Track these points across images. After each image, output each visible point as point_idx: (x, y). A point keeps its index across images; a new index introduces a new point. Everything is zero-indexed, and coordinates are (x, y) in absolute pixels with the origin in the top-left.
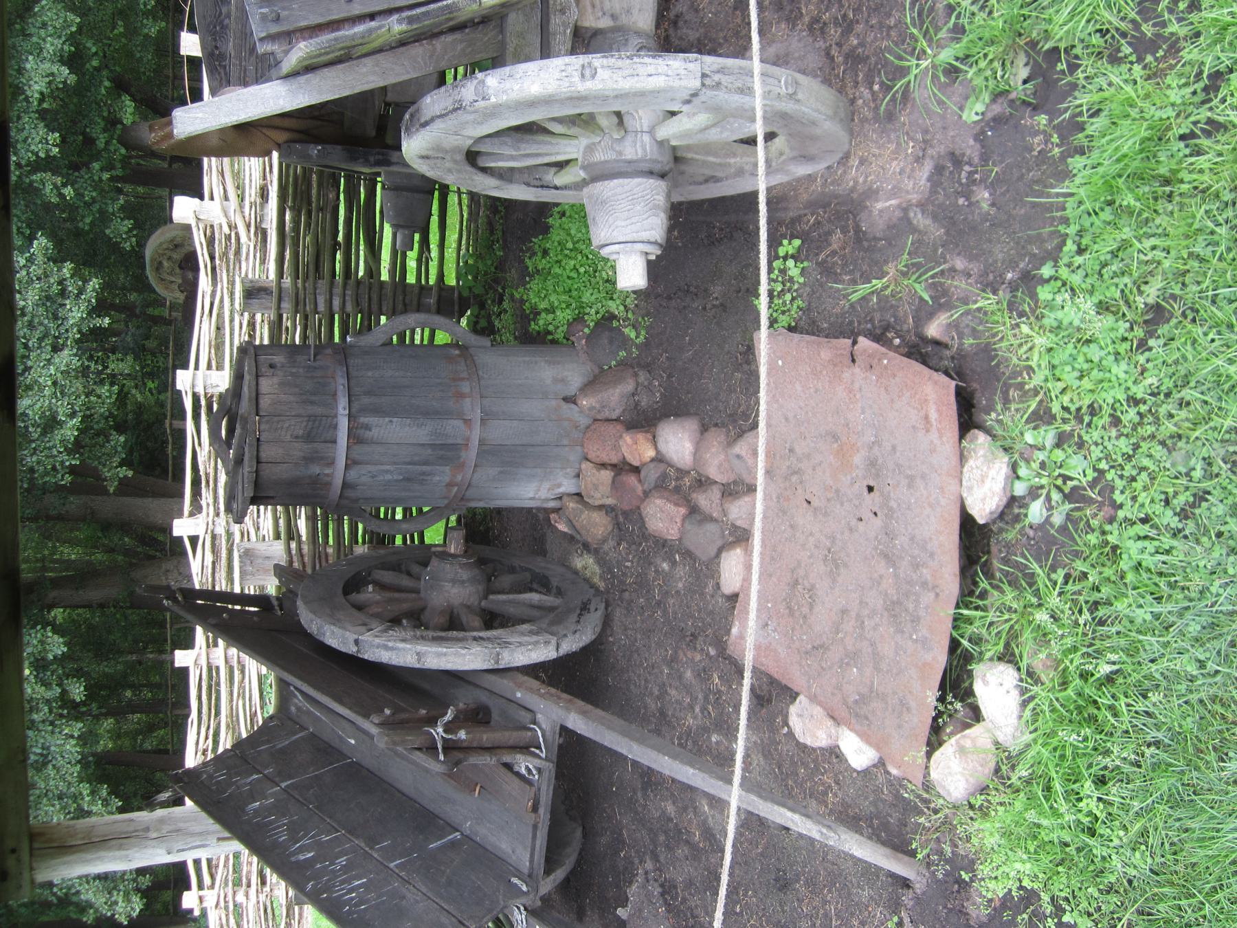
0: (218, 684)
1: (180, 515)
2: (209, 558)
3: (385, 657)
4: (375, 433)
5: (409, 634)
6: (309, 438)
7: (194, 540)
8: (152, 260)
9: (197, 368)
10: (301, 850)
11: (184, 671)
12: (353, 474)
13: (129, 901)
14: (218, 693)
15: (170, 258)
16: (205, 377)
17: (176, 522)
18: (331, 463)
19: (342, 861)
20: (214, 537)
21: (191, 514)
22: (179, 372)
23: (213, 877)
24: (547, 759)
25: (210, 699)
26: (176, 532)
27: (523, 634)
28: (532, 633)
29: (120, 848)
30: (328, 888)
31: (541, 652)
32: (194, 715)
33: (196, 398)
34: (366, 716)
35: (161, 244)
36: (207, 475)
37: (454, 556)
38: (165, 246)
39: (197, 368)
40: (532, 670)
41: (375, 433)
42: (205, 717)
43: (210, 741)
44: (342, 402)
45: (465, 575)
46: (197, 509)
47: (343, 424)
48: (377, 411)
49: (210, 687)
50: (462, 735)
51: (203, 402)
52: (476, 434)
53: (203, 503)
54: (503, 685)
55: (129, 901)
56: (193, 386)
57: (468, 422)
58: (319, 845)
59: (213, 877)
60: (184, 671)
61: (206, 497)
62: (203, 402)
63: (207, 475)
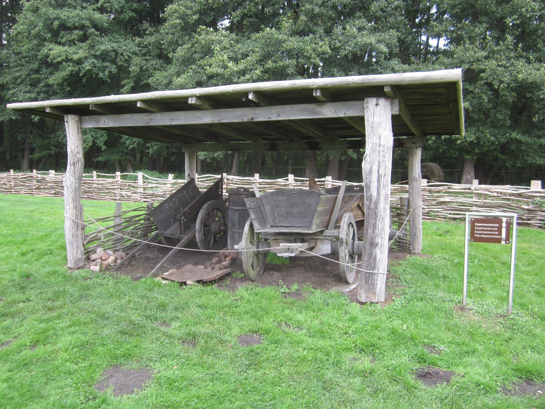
0: (250, 185)
1: (295, 176)
2: (282, 184)
3: (200, 213)
4: (236, 213)
5: (204, 217)
6: (235, 203)
7: (287, 180)
8: (427, 165)
9: (332, 182)
10: (175, 199)
11: (254, 176)
12: (230, 210)
13: (203, 156)
14: (247, 185)
15: (427, 171)
16: (330, 184)
17: (293, 175)
18: (232, 206)
19: (172, 205)
20: (288, 185)
21: (295, 179)
22: (331, 177)
23: (200, 181)
24: (178, 236)
25: (245, 182)
26: (289, 175)
27: (201, 236)
28: (202, 238)
29: (189, 167)
30: (167, 202)
31: (198, 239)
32: (242, 178)
33: (324, 181)
34: (188, 208)
35: (432, 168)
36: (305, 184)
37: (220, 228)
38: (432, 169)
39: (332, 182)
40: (195, 236)
41: (236, 213)
42: (241, 181)
43: (235, 182)
44: (241, 208)
45: (216, 229)
46: (296, 181)
47: (237, 208)
48: (239, 214)
49: (250, 183)
50: (182, 222)
51: (322, 183)
52: (236, 231)
53: (297, 183)
54: (193, 232)
55: (203, 156)
56: (327, 181)
57: (238, 229)
58: (175, 201)
59: (200, 181)
60: (254, 176)
61: (299, 183)
62: (322, 183)
63: (305, 184)
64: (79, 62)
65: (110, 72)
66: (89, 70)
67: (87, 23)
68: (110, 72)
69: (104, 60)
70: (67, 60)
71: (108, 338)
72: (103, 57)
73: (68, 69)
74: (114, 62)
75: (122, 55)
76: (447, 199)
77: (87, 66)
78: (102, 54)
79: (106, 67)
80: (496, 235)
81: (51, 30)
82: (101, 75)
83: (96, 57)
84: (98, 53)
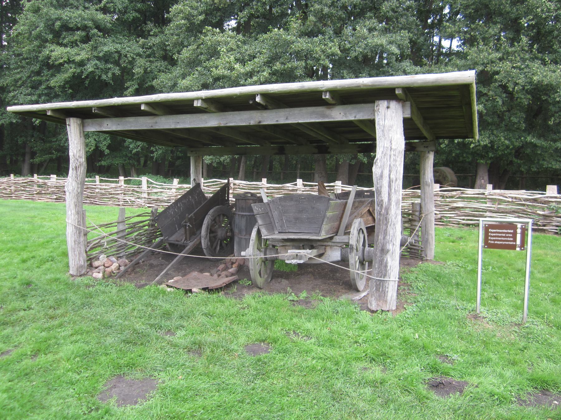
0: (257, 190)
1: (303, 181)
2: (290, 189)
3: (206, 219)
4: (243, 219)
5: (210, 223)
6: (242, 208)
7: (296, 185)
8: (439, 170)
9: (342, 187)
10: (180, 204)
11: (261, 181)
12: (237, 215)
13: (209, 160)
14: (255, 190)
15: (440, 176)
16: (339, 189)
17: (301, 180)
18: (239, 212)
19: (177, 210)
20: (297, 190)
21: (303, 184)
22: (341, 182)
23: (206, 186)
24: (184, 243)
25: (253, 187)
26: (298, 180)
27: (207, 242)
28: (207, 244)
29: (195, 172)
30: (172, 208)
31: (203, 246)
32: (249, 183)
33: (333, 186)
34: (194, 214)
35: (445, 173)
36: (314, 189)
37: (227, 234)
38: (445, 174)
39: (342, 187)
40: (200, 243)
41: (243, 219)
42: (248, 186)
43: (242, 187)
44: (248, 214)
45: (223, 235)
46: (305, 185)
47: (244, 214)
48: (246, 220)
49: (257, 187)
50: (187, 228)
51: (332, 188)
52: (243, 237)
53: (306, 188)
54: (198, 238)
55: (209, 160)
56: (337, 186)
57: (245, 236)
58: (180, 207)
59: (206, 186)
60: (261, 181)
61: (308, 188)
62: (332, 188)
63: (314, 189)
64: (82, 64)
65: (114, 74)
66: (92, 72)
67: (90, 24)
68: (114, 74)
69: (107, 62)
70: (69, 62)
71: (111, 347)
72: (106, 58)
73: (70, 71)
74: (117, 63)
75: (126, 56)
76: (460, 204)
77: (90, 68)
78: (105, 56)
79: (109, 69)
80: (511, 241)
81: (52, 31)
82: (104, 77)
83: (98, 58)
84: (101, 55)
